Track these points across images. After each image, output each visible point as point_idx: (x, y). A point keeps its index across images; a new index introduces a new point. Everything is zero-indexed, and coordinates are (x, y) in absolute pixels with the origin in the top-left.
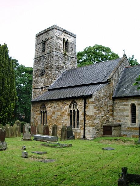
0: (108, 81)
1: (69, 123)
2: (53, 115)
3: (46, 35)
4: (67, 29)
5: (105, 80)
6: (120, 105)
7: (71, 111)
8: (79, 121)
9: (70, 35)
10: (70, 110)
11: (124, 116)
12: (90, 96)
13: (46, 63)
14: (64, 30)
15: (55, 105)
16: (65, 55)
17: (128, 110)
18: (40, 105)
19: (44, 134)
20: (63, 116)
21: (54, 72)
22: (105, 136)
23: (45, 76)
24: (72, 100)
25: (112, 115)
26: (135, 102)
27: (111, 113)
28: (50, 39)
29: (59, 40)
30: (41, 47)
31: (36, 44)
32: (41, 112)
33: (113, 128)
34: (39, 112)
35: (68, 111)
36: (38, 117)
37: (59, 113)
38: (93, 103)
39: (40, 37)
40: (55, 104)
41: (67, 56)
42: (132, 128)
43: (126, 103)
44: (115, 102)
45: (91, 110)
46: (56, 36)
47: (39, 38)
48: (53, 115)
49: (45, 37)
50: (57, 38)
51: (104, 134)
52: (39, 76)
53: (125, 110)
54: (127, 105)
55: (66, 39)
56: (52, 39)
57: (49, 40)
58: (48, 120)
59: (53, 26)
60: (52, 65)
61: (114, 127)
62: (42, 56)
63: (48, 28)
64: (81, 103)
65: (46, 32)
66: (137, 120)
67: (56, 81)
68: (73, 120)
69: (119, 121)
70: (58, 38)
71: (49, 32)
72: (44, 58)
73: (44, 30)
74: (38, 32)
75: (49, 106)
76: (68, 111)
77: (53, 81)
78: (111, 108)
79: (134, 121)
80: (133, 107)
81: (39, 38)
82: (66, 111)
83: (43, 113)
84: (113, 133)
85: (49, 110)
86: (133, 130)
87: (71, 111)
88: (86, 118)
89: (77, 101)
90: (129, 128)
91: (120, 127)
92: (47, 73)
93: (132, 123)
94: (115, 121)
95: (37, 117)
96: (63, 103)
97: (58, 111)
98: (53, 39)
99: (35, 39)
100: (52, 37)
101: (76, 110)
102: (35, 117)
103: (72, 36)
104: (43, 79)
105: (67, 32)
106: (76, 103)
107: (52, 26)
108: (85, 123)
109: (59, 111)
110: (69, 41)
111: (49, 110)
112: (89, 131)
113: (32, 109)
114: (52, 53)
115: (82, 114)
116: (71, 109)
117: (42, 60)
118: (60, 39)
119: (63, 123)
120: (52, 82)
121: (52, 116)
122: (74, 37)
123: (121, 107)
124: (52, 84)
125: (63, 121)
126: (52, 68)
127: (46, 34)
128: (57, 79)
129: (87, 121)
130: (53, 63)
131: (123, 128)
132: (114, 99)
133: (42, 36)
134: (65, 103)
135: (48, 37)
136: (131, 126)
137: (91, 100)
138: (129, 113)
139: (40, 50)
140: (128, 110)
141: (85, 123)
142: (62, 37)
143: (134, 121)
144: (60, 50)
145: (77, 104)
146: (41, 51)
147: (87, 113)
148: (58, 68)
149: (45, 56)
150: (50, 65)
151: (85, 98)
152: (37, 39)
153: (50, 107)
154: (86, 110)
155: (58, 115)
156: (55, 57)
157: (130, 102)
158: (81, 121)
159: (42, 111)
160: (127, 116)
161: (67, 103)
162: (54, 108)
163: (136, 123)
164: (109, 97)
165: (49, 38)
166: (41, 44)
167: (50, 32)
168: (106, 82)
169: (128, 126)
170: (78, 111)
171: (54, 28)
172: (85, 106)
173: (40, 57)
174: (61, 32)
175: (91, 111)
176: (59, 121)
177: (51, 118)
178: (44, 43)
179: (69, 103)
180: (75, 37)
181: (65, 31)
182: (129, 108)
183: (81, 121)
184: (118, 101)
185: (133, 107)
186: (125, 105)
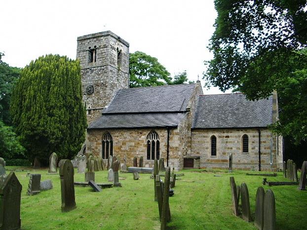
0: (188, 110)
1: (146, 155)
2: (123, 146)
3: (95, 41)
4: (122, 37)
5: (184, 110)
6: (199, 137)
7: (149, 141)
8: (161, 153)
9: (124, 44)
10: (147, 140)
11: (203, 148)
12: (176, 127)
13: (97, 79)
14: (119, 38)
15: (127, 135)
16: (119, 70)
17: (208, 142)
18: (102, 133)
19: (134, 166)
20: (138, 147)
21: (108, 91)
22: (186, 168)
23: (94, 95)
24: (150, 130)
25: (190, 146)
26: (216, 134)
27: (189, 144)
28: (102, 48)
29: (113, 50)
30: (87, 57)
31: (77, 50)
32: (103, 143)
33: (195, 160)
34: (100, 142)
35: (145, 142)
36: (99, 148)
37: (133, 144)
38: (177, 134)
39: (86, 42)
40: (125, 133)
41: (120, 71)
42: (212, 161)
43: (205, 134)
44: (193, 133)
45: (176, 142)
46: (111, 46)
47: (83, 43)
48: (123, 146)
49: (93, 44)
50: (111, 48)
51: (184, 167)
52: (85, 95)
53: (204, 142)
54: (207, 137)
55: (119, 49)
56: (105, 49)
57: (101, 49)
58: (115, 151)
59: (108, 32)
60: (106, 82)
61: (196, 159)
62: (89, 69)
63: (100, 33)
64: (163, 135)
65: (96, 37)
66: (217, 152)
67: (110, 102)
68: (109, 150)
69: (198, 153)
70: (113, 48)
71: (100, 38)
72: (92, 71)
73: (93, 35)
74: (82, 34)
75: (117, 134)
76: (145, 142)
77: (107, 102)
78: (190, 139)
79: (214, 153)
80: (214, 139)
81: (83, 43)
82: (143, 141)
83: (110, 144)
84: (194, 166)
85: (117, 140)
86: (213, 162)
87: (149, 141)
88: (170, 150)
89: (158, 132)
90: (208, 160)
91: (134, 164)
92: (98, 92)
93: (212, 155)
94: (193, 153)
95: (97, 148)
96: (138, 133)
97: (130, 141)
98: (108, 48)
99: (77, 44)
100: (105, 46)
101: (155, 141)
102: (93, 148)
103: (125, 45)
104: (90, 99)
105: (121, 40)
106: (156, 133)
107: (105, 32)
108: (168, 155)
109: (132, 142)
110: (123, 52)
111: (117, 140)
112: (173, 163)
113: (89, 138)
114: (105, 67)
115: (164, 146)
116: (149, 139)
117: (89, 74)
118: (114, 49)
119: (139, 154)
120: (105, 104)
121: (121, 147)
122: (127, 46)
123: (200, 139)
124: (106, 107)
125: (138, 153)
126: (106, 87)
127: (95, 39)
128: (112, 100)
129: (171, 153)
130: (107, 80)
131: (202, 160)
132: (192, 130)
133: (89, 41)
134: (141, 133)
135: (99, 45)
136: (211, 159)
137: (175, 131)
138: (209, 145)
139: (85, 60)
140: (208, 142)
141: (168, 155)
142: (116, 47)
143: (214, 153)
144: (114, 64)
145: (157, 134)
146: (87, 62)
147: (170, 145)
148: (113, 86)
149: (95, 69)
150: (102, 81)
151: (170, 129)
152: (80, 43)
153: (118, 137)
154: (170, 141)
155: (131, 146)
156: (110, 73)
157: (211, 134)
158: (163, 153)
159: (105, 141)
160: (207, 148)
161: (144, 133)
162: (125, 138)
163: (216, 155)
164: (188, 128)
165: (100, 46)
166: (88, 52)
167: (102, 38)
168: (185, 112)
169: (208, 158)
170: (158, 142)
171: (109, 35)
172: (168, 137)
173: (87, 69)
174: (115, 40)
175: (175, 142)
176: (132, 153)
177: (120, 148)
178: (92, 51)
179: (147, 133)
180: (128, 47)
181: (119, 39)
182: (209, 140)
183: (163, 153)
184: (197, 132)
185: (214, 139)
186: (204, 137)
